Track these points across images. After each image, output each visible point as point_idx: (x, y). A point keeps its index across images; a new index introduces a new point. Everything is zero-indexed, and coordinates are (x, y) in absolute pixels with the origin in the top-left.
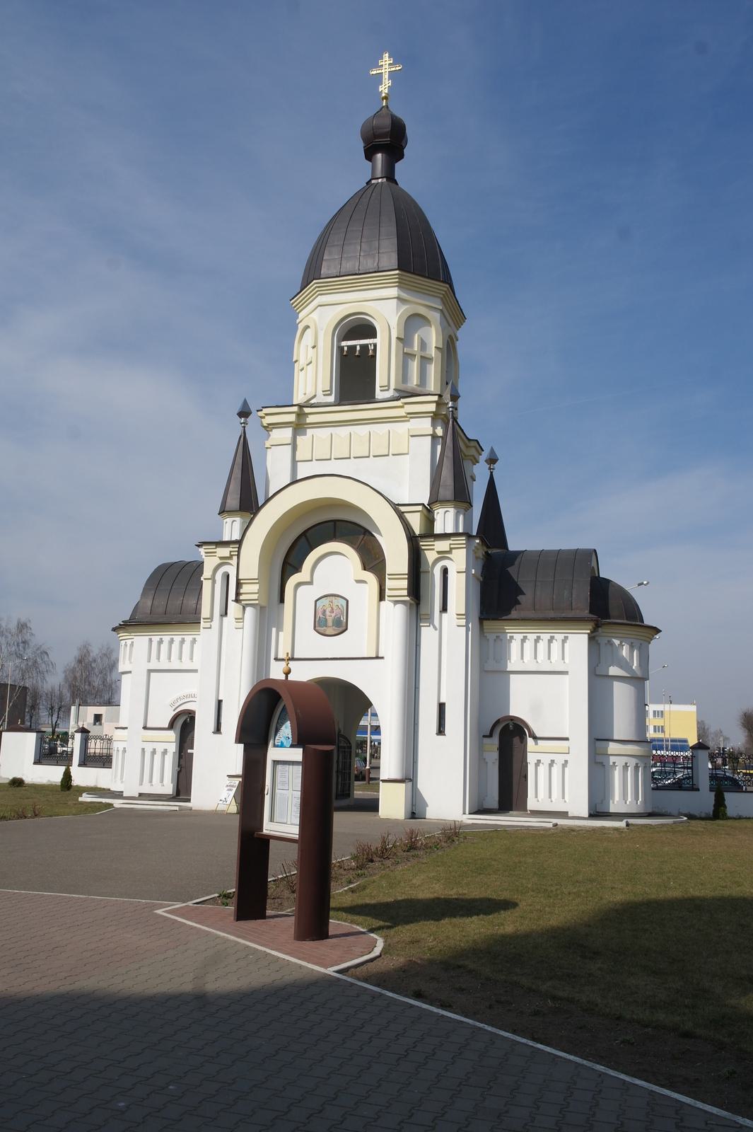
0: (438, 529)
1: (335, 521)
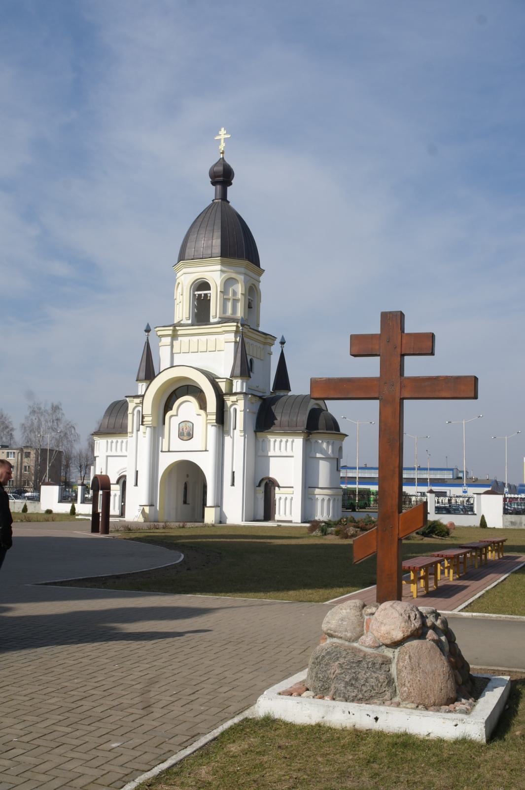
0: (234, 391)
1: (188, 386)
